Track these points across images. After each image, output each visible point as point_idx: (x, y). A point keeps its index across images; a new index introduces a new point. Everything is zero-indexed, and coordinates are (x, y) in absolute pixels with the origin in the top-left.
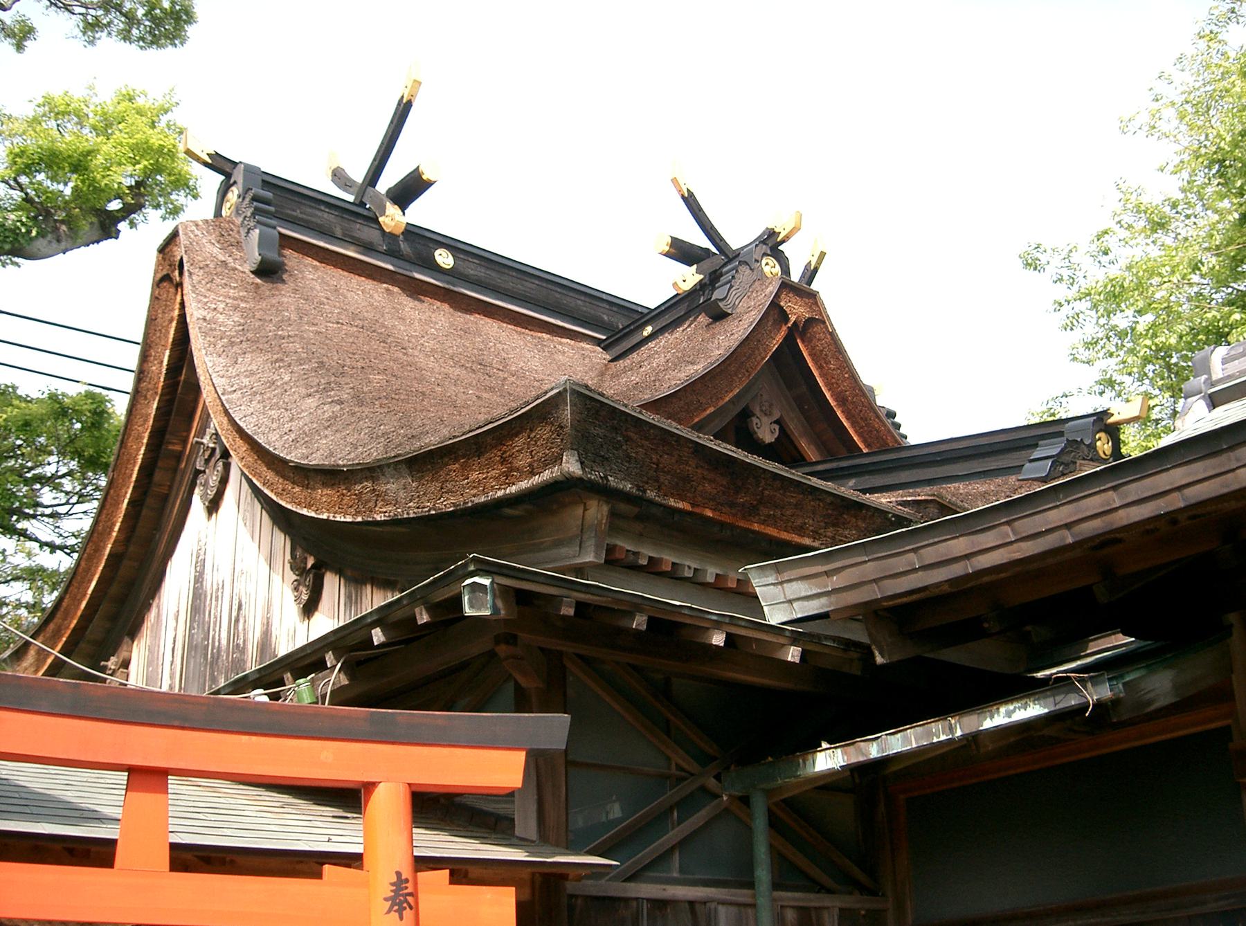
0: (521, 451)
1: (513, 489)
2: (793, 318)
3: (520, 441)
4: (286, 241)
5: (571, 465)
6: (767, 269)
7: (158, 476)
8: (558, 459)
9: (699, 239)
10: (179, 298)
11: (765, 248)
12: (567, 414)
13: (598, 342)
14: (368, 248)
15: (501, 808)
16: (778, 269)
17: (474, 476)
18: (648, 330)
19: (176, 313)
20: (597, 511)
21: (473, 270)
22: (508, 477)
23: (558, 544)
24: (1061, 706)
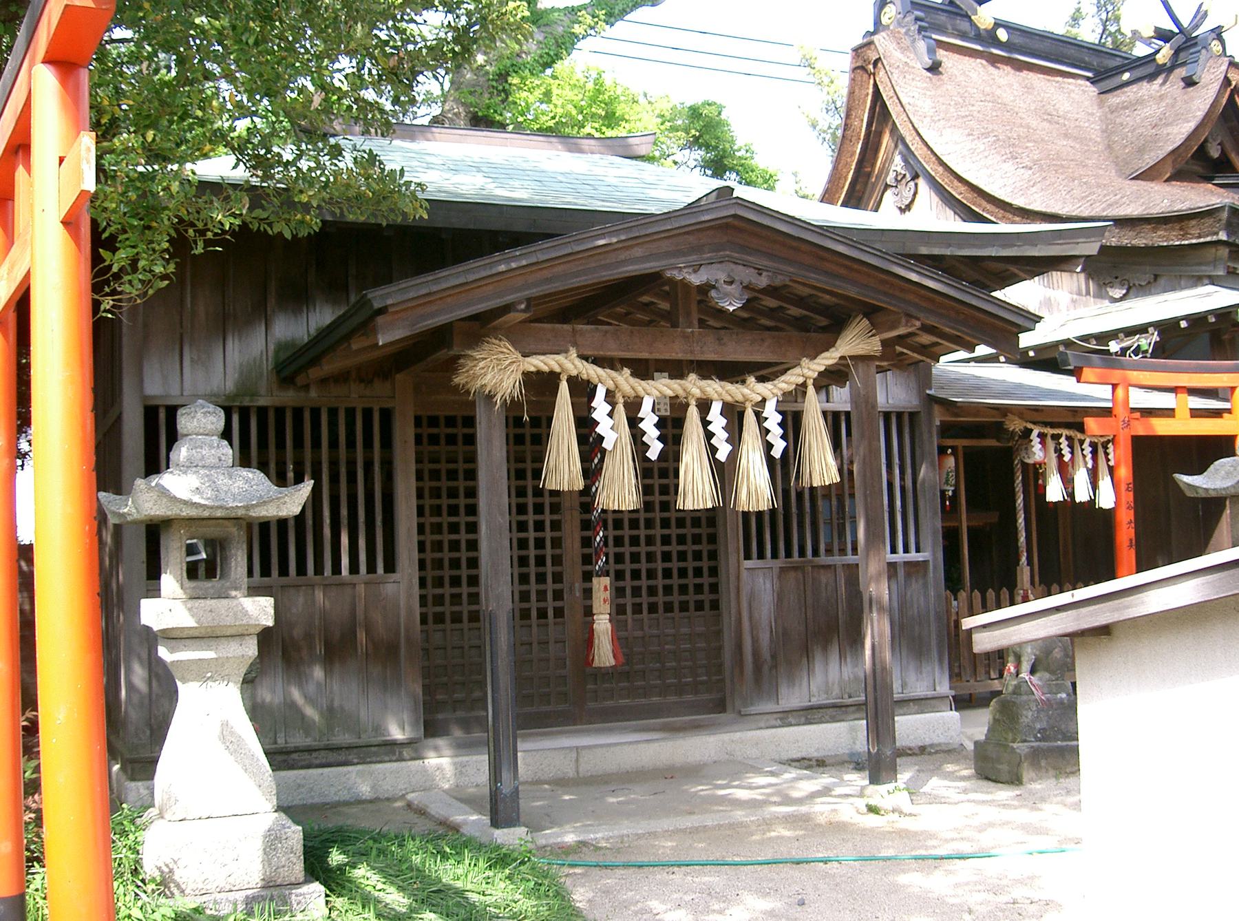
0: (1194, 226)
1: (1186, 242)
2: (1234, 83)
3: (1193, 222)
4: (941, 44)
5: (1223, 236)
6: (1215, 49)
7: (858, 187)
8: (1217, 234)
9: (1169, 25)
10: (872, 81)
11: (1214, 35)
12: (1225, 215)
13: (1088, 79)
14: (963, 36)
15: (830, 418)
16: (1220, 48)
17: (1159, 233)
18: (1126, 76)
19: (871, 91)
20: (1224, 252)
21: (1018, 40)
22: (1184, 237)
23: (1200, 264)
24: (1125, 242)
